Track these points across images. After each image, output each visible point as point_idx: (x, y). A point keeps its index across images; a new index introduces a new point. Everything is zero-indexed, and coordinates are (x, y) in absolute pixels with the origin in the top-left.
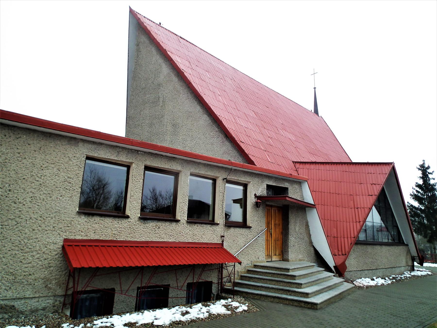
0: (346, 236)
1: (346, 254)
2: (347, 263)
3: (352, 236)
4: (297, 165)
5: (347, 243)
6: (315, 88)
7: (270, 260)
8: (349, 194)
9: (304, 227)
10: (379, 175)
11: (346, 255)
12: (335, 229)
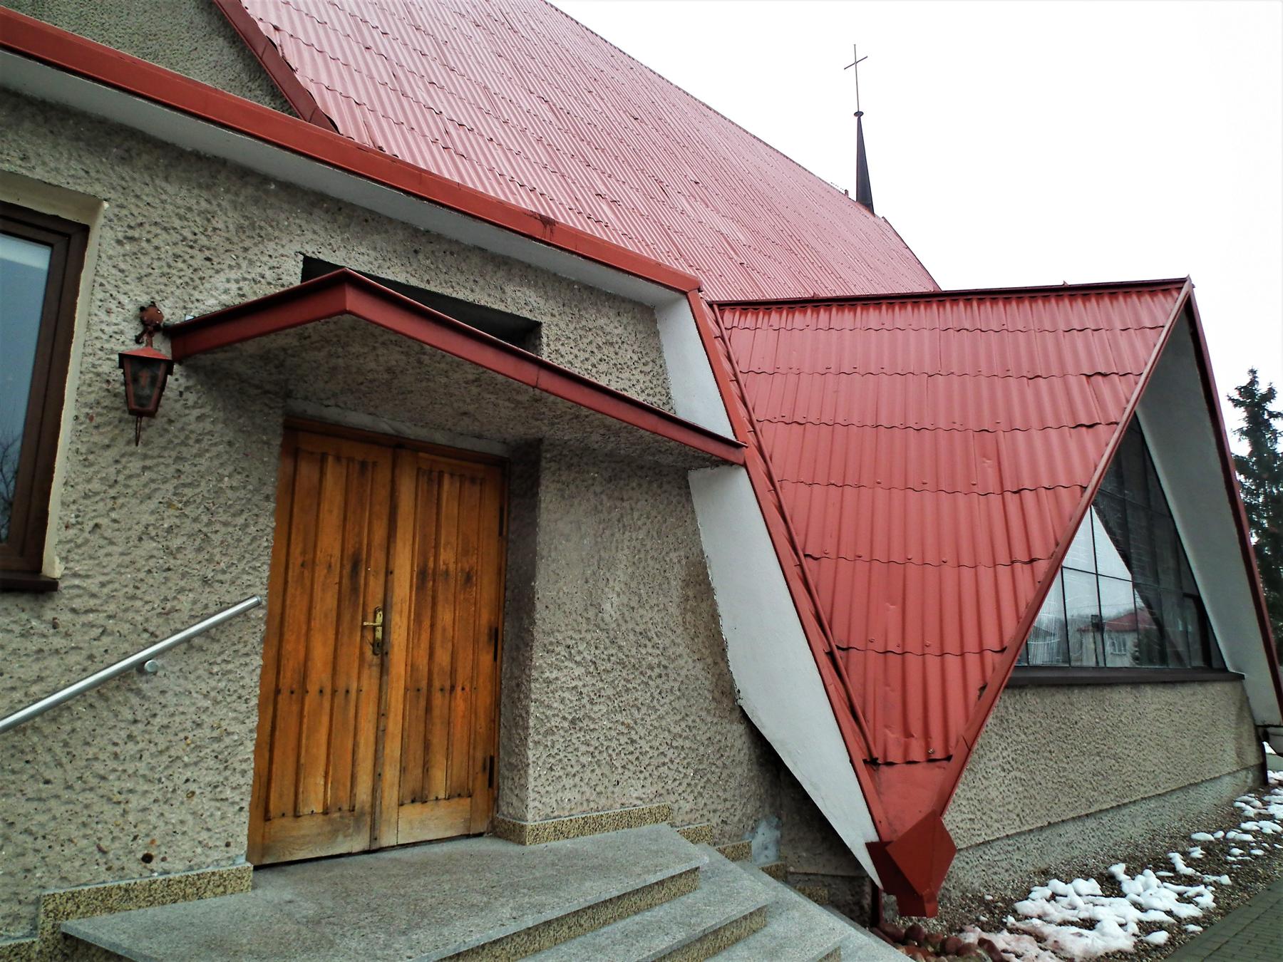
0: (952, 645)
1: (949, 758)
2: (953, 820)
3: (991, 642)
4: (729, 318)
5: (957, 682)
6: (859, 114)
7: (359, 843)
8: (972, 425)
9: (676, 594)
10: (1123, 340)
11: (953, 760)
12: (894, 609)
